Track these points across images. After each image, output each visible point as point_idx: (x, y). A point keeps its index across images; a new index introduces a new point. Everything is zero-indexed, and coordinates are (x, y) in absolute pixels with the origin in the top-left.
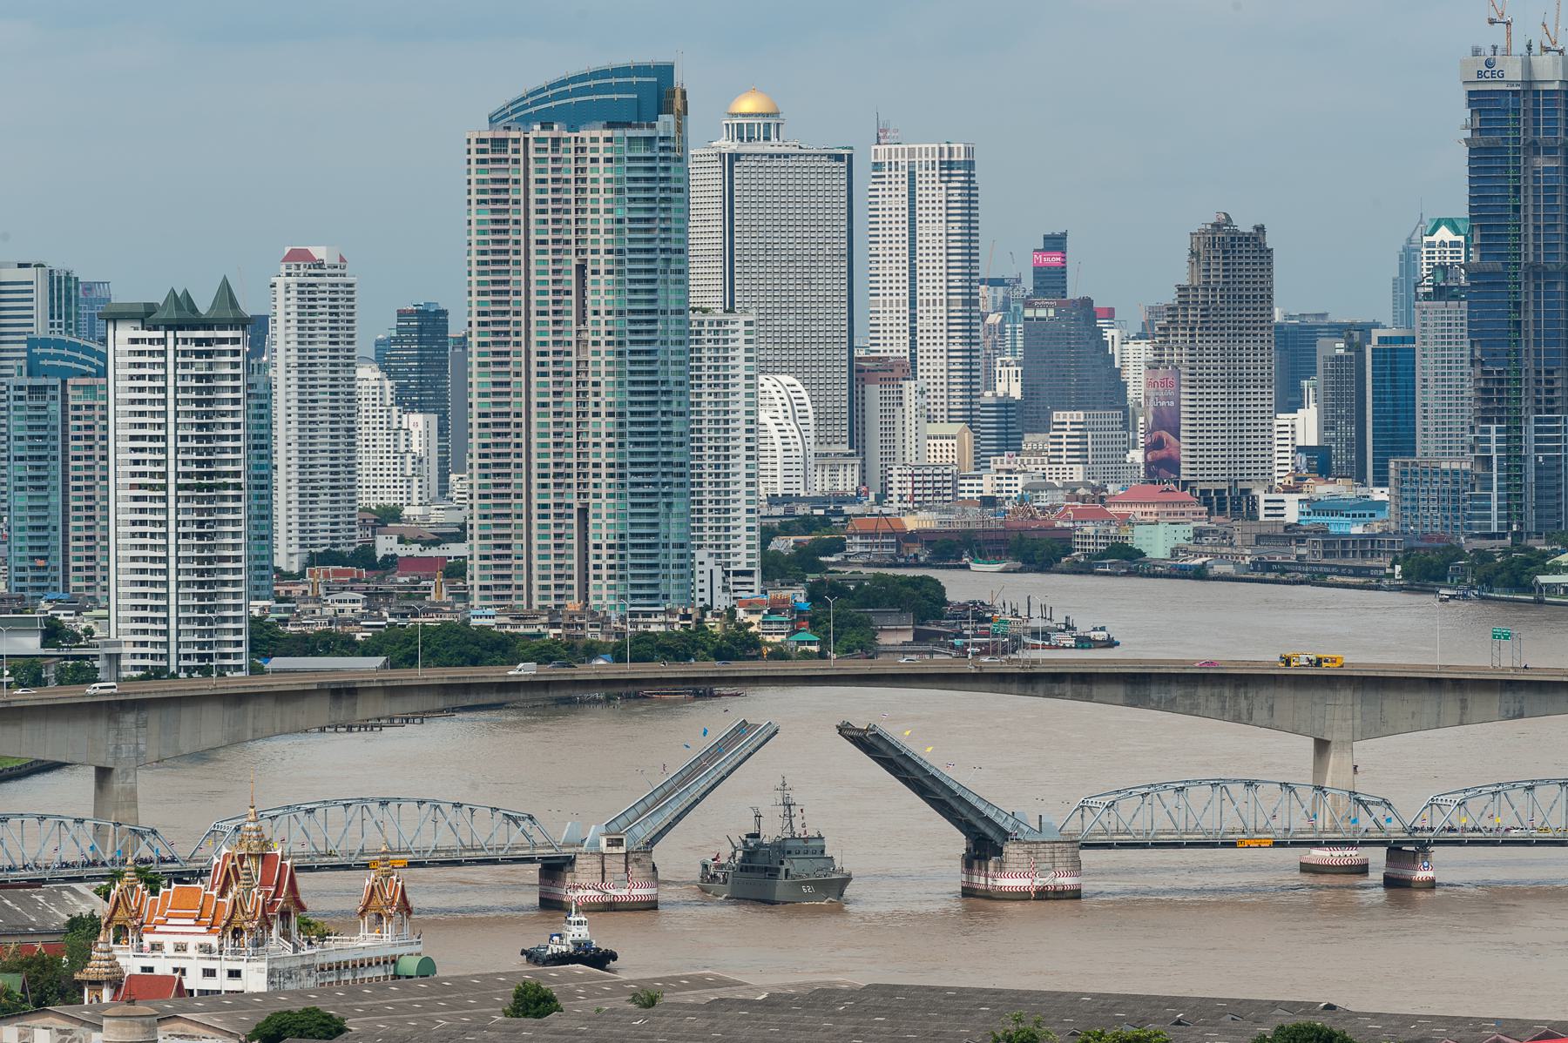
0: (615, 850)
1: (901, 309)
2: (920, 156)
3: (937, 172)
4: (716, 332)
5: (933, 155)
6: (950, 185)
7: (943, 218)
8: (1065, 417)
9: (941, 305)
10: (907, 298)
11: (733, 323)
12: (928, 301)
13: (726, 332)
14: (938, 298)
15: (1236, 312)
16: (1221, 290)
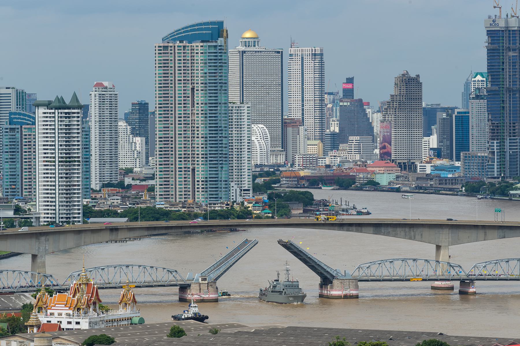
0: (204, 282)
1: (299, 102)
3: (311, 57)
4: (238, 110)
5: (310, 52)
6: (315, 61)
7: (313, 72)
8: (353, 138)
9: (312, 101)
10: (301, 99)
11: (243, 107)
13: (241, 110)
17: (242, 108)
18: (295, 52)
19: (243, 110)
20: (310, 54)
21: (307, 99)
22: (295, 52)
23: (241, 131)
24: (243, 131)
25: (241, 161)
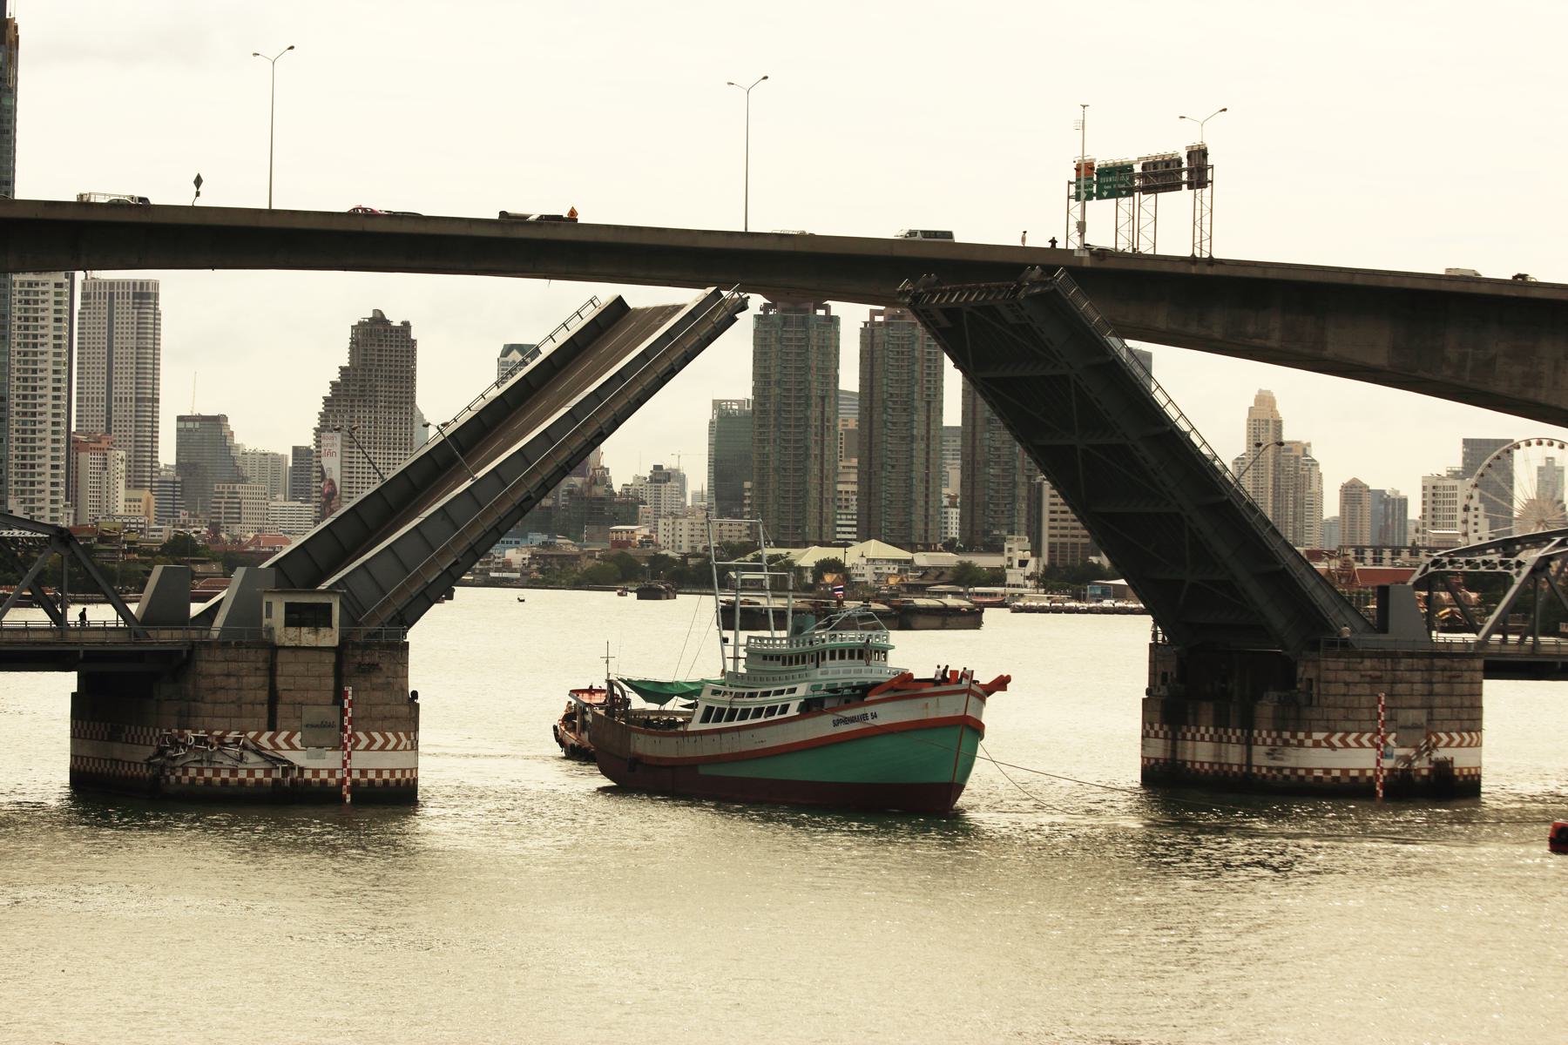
0: (307, 637)
1: (100, 404)
2: (118, 288)
3: (131, 301)
4: (27, 293)
5: (128, 288)
6: (142, 311)
7: (135, 336)
8: (223, 488)
9: (131, 401)
10: (105, 396)
11: (43, 284)
12: (121, 398)
13: (36, 293)
14: (128, 396)
15: (398, 390)
16: (376, 370)
17: (41, 288)
18: (95, 289)
19: (43, 293)
20: (128, 293)
21: (118, 396)
22: (95, 289)
23: (35, 354)
24: (42, 353)
25: (33, 440)
